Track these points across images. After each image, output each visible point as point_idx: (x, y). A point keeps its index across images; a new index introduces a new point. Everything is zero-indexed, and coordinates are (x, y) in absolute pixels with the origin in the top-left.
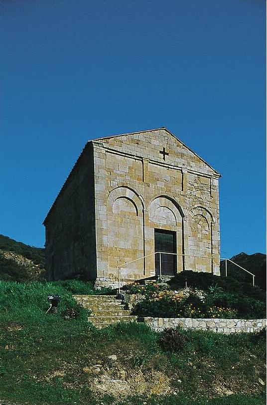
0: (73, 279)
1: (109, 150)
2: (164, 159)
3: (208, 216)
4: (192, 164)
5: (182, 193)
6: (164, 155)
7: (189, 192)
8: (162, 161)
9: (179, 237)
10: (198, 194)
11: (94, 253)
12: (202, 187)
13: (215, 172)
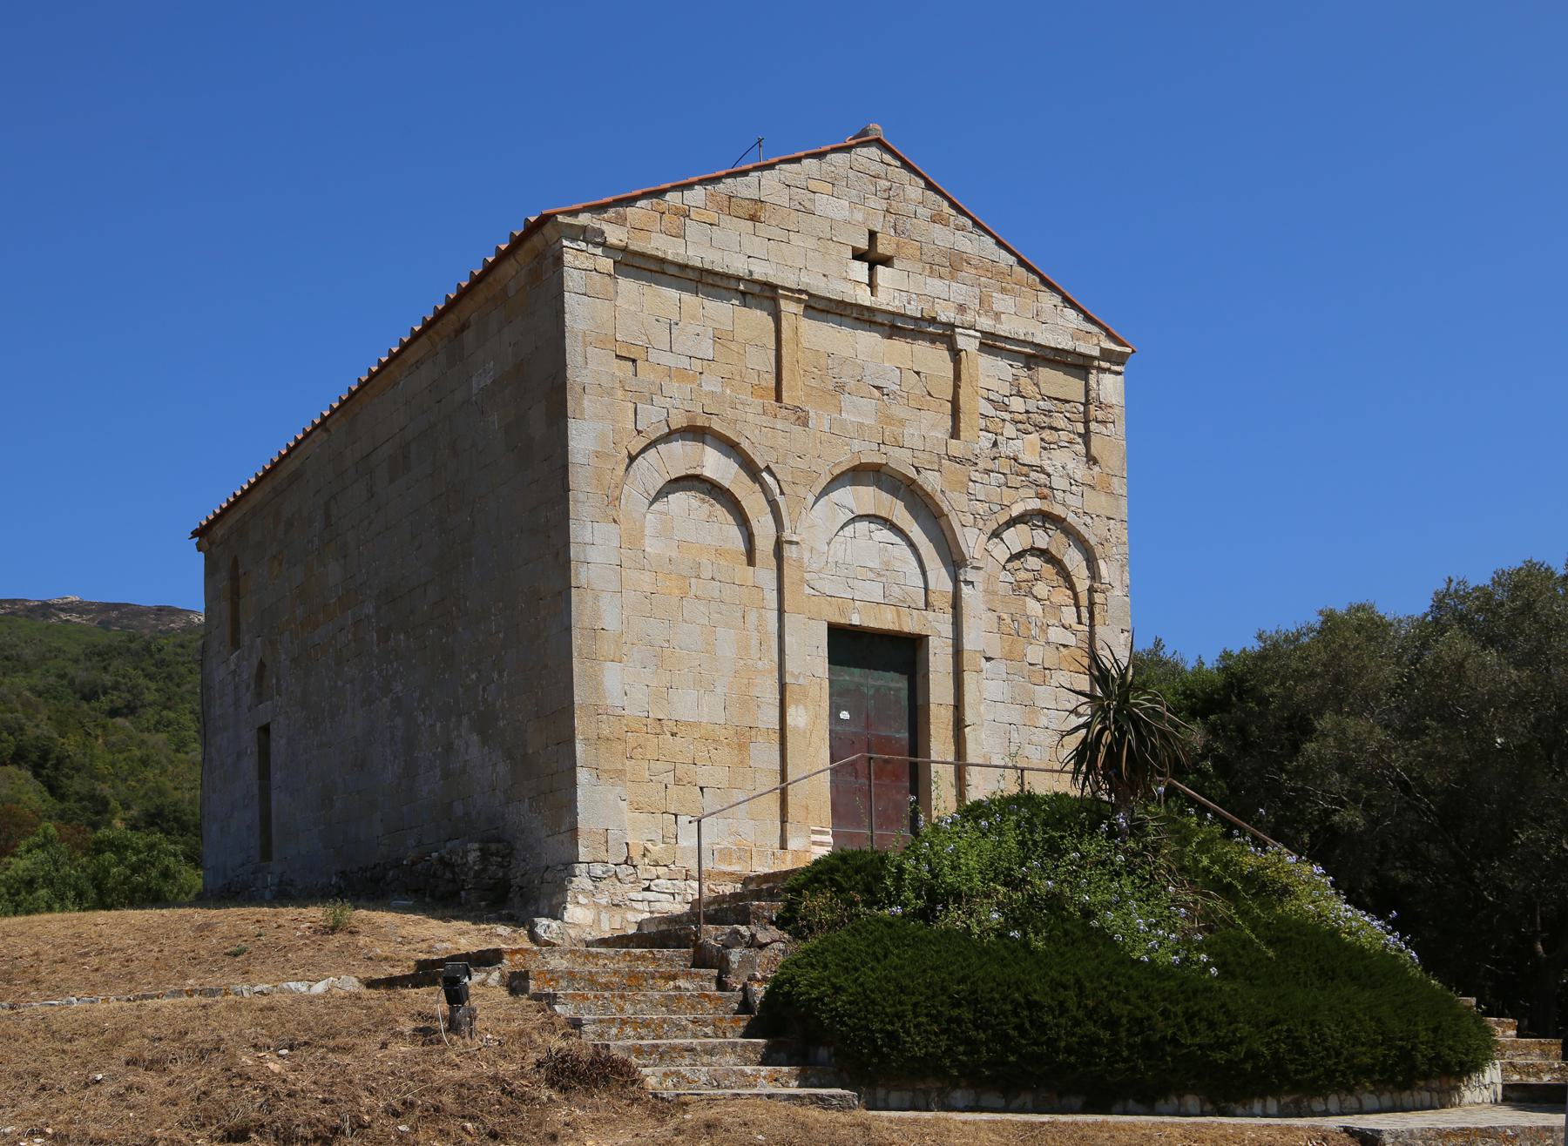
1: (630, 260)
2: (872, 284)
3: (1073, 559)
4: (1002, 302)
6: (871, 269)
8: (864, 297)
9: (1533, 1119)
10: (1027, 448)
11: (880, 1104)
12: (1048, 413)
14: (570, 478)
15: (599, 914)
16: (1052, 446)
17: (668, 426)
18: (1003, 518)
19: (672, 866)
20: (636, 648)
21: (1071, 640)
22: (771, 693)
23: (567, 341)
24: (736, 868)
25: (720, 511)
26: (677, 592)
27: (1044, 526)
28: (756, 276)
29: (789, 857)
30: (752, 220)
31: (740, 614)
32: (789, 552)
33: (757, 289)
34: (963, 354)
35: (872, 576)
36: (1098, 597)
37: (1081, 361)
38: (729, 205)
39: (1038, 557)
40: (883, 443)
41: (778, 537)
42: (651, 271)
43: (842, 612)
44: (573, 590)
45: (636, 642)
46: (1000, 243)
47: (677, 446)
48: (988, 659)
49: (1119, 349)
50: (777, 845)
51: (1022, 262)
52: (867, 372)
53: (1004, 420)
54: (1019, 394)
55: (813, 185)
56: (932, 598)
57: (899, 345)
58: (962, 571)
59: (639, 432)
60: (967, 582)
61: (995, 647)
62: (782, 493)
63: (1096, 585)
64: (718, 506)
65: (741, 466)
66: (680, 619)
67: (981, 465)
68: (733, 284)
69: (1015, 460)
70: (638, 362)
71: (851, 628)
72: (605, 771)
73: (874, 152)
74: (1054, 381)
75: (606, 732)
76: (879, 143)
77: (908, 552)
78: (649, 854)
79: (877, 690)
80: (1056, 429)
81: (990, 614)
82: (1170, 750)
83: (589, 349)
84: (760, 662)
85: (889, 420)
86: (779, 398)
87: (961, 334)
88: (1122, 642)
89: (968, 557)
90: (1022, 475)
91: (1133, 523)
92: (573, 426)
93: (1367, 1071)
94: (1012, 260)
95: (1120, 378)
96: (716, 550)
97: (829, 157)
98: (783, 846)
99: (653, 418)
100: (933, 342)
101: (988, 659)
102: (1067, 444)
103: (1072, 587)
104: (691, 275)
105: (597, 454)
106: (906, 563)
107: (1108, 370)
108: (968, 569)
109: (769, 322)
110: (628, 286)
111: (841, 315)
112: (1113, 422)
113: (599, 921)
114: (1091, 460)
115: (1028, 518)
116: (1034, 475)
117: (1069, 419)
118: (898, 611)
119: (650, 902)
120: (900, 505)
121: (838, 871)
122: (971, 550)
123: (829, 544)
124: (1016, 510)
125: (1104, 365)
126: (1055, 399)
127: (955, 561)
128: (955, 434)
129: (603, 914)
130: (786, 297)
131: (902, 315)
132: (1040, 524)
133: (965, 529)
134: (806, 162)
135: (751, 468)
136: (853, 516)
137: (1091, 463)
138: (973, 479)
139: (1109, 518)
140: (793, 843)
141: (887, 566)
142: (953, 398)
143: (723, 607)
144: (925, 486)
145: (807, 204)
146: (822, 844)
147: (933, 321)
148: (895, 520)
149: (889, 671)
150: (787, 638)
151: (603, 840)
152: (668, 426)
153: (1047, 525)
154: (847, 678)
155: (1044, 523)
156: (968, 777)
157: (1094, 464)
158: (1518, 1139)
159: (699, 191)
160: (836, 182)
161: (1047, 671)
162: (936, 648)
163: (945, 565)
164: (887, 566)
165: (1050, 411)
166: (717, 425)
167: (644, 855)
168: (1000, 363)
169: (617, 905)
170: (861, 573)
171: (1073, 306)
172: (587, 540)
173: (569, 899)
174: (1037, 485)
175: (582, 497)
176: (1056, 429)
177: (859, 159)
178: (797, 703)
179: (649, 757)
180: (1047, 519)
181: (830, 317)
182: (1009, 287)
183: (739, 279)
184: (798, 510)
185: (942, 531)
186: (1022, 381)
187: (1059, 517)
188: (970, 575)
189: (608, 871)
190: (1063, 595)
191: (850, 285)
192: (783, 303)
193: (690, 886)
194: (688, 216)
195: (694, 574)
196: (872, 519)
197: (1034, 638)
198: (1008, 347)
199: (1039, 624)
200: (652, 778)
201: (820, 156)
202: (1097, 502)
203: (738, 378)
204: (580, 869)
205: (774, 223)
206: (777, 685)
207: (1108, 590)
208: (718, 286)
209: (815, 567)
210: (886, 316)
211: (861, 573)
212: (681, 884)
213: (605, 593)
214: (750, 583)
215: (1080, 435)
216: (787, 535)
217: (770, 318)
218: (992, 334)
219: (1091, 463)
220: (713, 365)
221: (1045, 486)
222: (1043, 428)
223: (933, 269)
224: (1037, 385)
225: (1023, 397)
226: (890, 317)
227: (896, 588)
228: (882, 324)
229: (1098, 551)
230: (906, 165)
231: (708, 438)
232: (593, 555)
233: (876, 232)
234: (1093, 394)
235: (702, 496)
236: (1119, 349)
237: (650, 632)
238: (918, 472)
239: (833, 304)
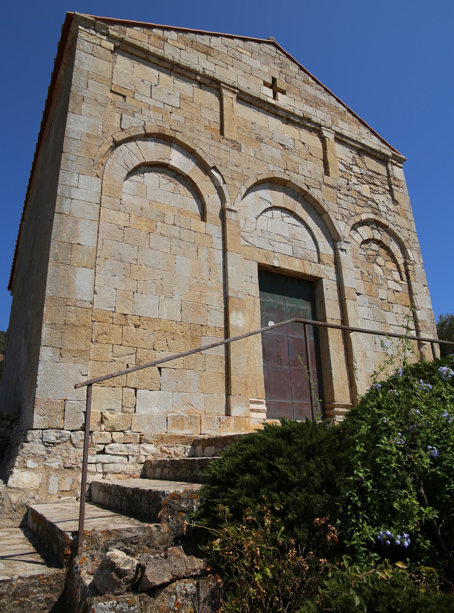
3: (394, 247)
10: (365, 190)
14: (64, 145)
15: (48, 477)
16: (376, 192)
17: (145, 130)
18: (358, 220)
19: (129, 431)
20: (107, 262)
22: (218, 302)
23: (74, 73)
24: (187, 431)
25: (182, 188)
26: (146, 229)
27: (378, 229)
28: (207, 72)
29: (232, 422)
31: (194, 249)
32: (228, 215)
33: (208, 81)
35: (285, 241)
36: (410, 267)
40: (287, 169)
41: (222, 207)
43: (267, 258)
44: (56, 215)
45: (109, 257)
46: (338, 100)
47: (151, 145)
48: (358, 294)
50: (223, 412)
53: (351, 175)
54: (356, 165)
56: (322, 257)
58: (338, 244)
59: (122, 129)
60: (342, 250)
61: (361, 287)
62: (224, 182)
63: (408, 261)
64: (181, 186)
65: (197, 164)
68: (193, 76)
70: (127, 98)
71: (274, 271)
72: (68, 351)
75: (73, 318)
76: (273, 44)
77: (306, 231)
78: (106, 422)
81: (356, 269)
83: (90, 81)
84: (210, 282)
86: (222, 133)
87: (324, 130)
88: (425, 291)
89: (341, 236)
91: (419, 233)
92: (71, 118)
94: (345, 109)
95: (401, 170)
96: (179, 210)
98: (228, 413)
100: (310, 131)
101: (358, 294)
102: (382, 193)
103: (395, 262)
104: (166, 65)
105: (88, 136)
106: (305, 237)
108: (342, 242)
109: (217, 100)
113: (47, 484)
114: (395, 202)
115: (369, 223)
116: (370, 202)
117: (382, 182)
118: (302, 262)
119: (103, 464)
121: (280, 455)
122: (343, 232)
123: (257, 218)
124: (364, 217)
128: (327, 173)
129: (53, 477)
130: (226, 89)
132: (375, 227)
133: (338, 221)
136: (271, 206)
137: (395, 203)
138: (339, 197)
139: (408, 230)
140: (235, 411)
142: (324, 158)
143: (181, 243)
144: (313, 195)
146: (258, 411)
147: (309, 120)
148: (296, 212)
150: (229, 268)
151: (61, 409)
152: (145, 130)
153: (379, 229)
154: (272, 301)
155: (377, 227)
156: (354, 364)
157: (397, 204)
160: (253, 53)
161: (390, 304)
162: (327, 286)
165: (372, 176)
166: (179, 137)
167: (102, 422)
168: (345, 149)
169: (70, 468)
170: (278, 238)
171: (376, 135)
172: (73, 184)
173: (17, 464)
174: (372, 208)
178: (238, 310)
179: (113, 342)
180: (378, 225)
181: (252, 106)
184: (235, 193)
185: (324, 222)
187: (385, 225)
189: (61, 437)
190: (391, 265)
192: (224, 91)
193: (144, 449)
194: (167, 42)
195: (159, 220)
196: (283, 210)
197: (381, 285)
199: (383, 278)
200: (115, 358)
204: (33, 435)
206: (222, 298)
209: (248, 229)
211: (278, 238)
212: (135, 447)
213: (84, 220)
214: (203, 231)
216: (228, 205)
217: (217, 98)
219: (395, 203)
220: (179, 111)
226: (287, 114)
229: (406, 244)
230: (288, 57)
231: (227, 296)
232: (76, 194)
234: (391, 173)
235: (169, 178)
237: (121, 252)
238: (308, 188)
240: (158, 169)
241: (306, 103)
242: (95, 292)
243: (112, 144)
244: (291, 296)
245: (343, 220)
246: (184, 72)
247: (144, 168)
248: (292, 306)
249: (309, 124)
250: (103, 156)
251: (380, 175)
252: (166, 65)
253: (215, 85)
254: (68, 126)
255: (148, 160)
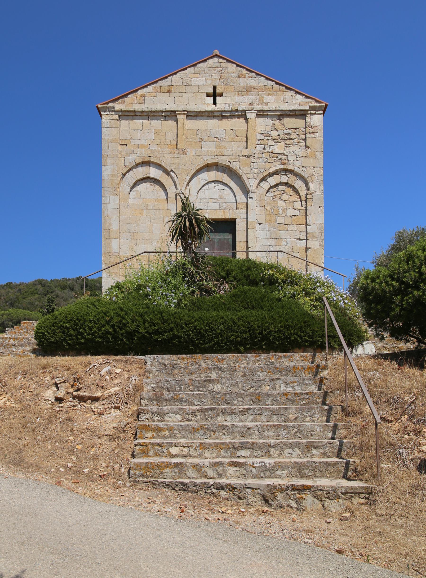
0: (297, 304)
1: (124, 114)
3: (299, 184)
4: (267, 99)
5: (246, 152)
7: (260, 148)
8: (212, 108)
10: (279, 148)
13: (317, 101)
21: (297, 213)
28: (167, 109)
30: (168, 92)
33: (169, 114)
34: (249, 120)
35: (215, 201)
36: (308, 197)
37: (302, 113)
38: (160, 90)
39: (284, 186)
42: (132, 116)
47: (140, 169)
49: (318, 105)
51: (277, 83)
52: (212, 133)
53: (268, 140)
55: (191, 76)
57: (225, 122)
59: (125, 166)
60: (250, 198)
61: (262, 219)
62: (177, 178)
64: (157, 186)
66: (140, 223)
67: (256, 156)
68: (160, 114)
69: (272, 153)
73: (216, 59)
74: (290, 122)
77: (230, 191)
79: (220, 240)
80: (292, 139)
82: (197, 229)
85: (221, 147)
90: (275, 157)
91: (326, 168)
92: (103, 168)
93: (241, 344)
94: (273, 83)
97: (198, 65)
99: (130, 161)
100: (239, 118)
103: (299, 195)
104: (145, 114)
105: (111, 175)
107: (315, 114)
108: (251, 193)
110: (124, 122)
111: (202, 116)
112: (318, 132)
114: (307, 147)
115: (279, 172)
116: (280, 157)
118: (224, 212)
120: (225, 176)
124: (271, 170)
125: (312, 112)
126: (292, 128)
127: (246, 191)
130: (179, 114)
131: (225, 111)
133: (249, 180)
134: (188, 69)
135: (167, 172)
141: (221, 197)
143: (156, 217)
144: (233, 167)
145: (189, 83)
147: (237, 111)
148: (223, 181)
149: (224, 233)
158: (225, 361)
159: (150, 87)
163: (244, 194)
164: (221, 197)
165: (289, 133)
166: (152, 159)
171: (300, 94)
172: (108, 202)
175: (106, 189)
176: (292, 139)
177: (210, 63)
180: (287, 171)
181: (198, 117)
182: (271, 93)
183: (162, 112)
186: (276, 125)
187: (291, 170)
188: (250, 195)
191: (206, 106)
192: (178, 116)
196: (215, 182)
198: (269, 113)
201: (194, 66)
202: (311, 162)
203: (163, 144)
205: (176, 91)
207: (313, 193)
208: (156, 116)
210: (218, 113)
214: (166, 209)
215: (303, 139)
218: (262, 110)
220: (154, 141)
221: (285, 160)
222: (286, 140)
223: (239, 93)
224: (283, 125)
225: (277, 130)
227: (225, 204)
228: (218, 116)
229: (309, 180)
230: (228, 61)
232: (109, 206)
233: (216, 86)
234: (308, 124)
236: (318, 105)
237: (129, 228)
238: (230, 163)
239: (198, 113)
240: (145, 180)
241: (239, 95)
242: (120, 248)
243: (122, 176)
244: (219, 233)
245: (253, 177)
246: (155, 114)
247: (139, 182)
248: (220, 237)
249: (237, 114)
250: (118, 184)
251: (298, 128)
252: (145, 114)
253: (173, 114)
254: (103, 173)
255: (139, 178)
